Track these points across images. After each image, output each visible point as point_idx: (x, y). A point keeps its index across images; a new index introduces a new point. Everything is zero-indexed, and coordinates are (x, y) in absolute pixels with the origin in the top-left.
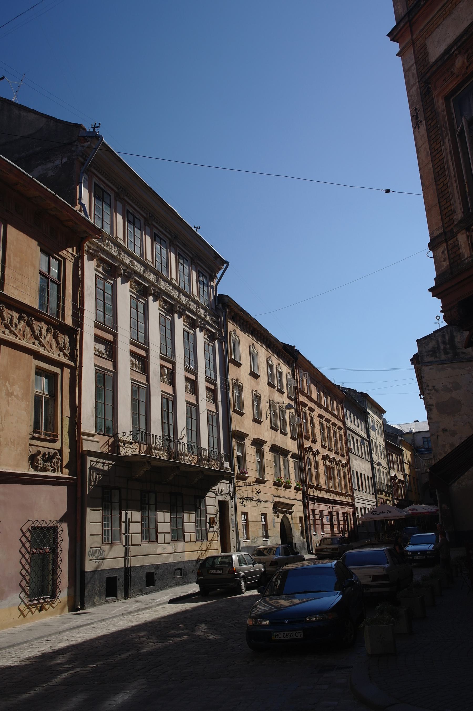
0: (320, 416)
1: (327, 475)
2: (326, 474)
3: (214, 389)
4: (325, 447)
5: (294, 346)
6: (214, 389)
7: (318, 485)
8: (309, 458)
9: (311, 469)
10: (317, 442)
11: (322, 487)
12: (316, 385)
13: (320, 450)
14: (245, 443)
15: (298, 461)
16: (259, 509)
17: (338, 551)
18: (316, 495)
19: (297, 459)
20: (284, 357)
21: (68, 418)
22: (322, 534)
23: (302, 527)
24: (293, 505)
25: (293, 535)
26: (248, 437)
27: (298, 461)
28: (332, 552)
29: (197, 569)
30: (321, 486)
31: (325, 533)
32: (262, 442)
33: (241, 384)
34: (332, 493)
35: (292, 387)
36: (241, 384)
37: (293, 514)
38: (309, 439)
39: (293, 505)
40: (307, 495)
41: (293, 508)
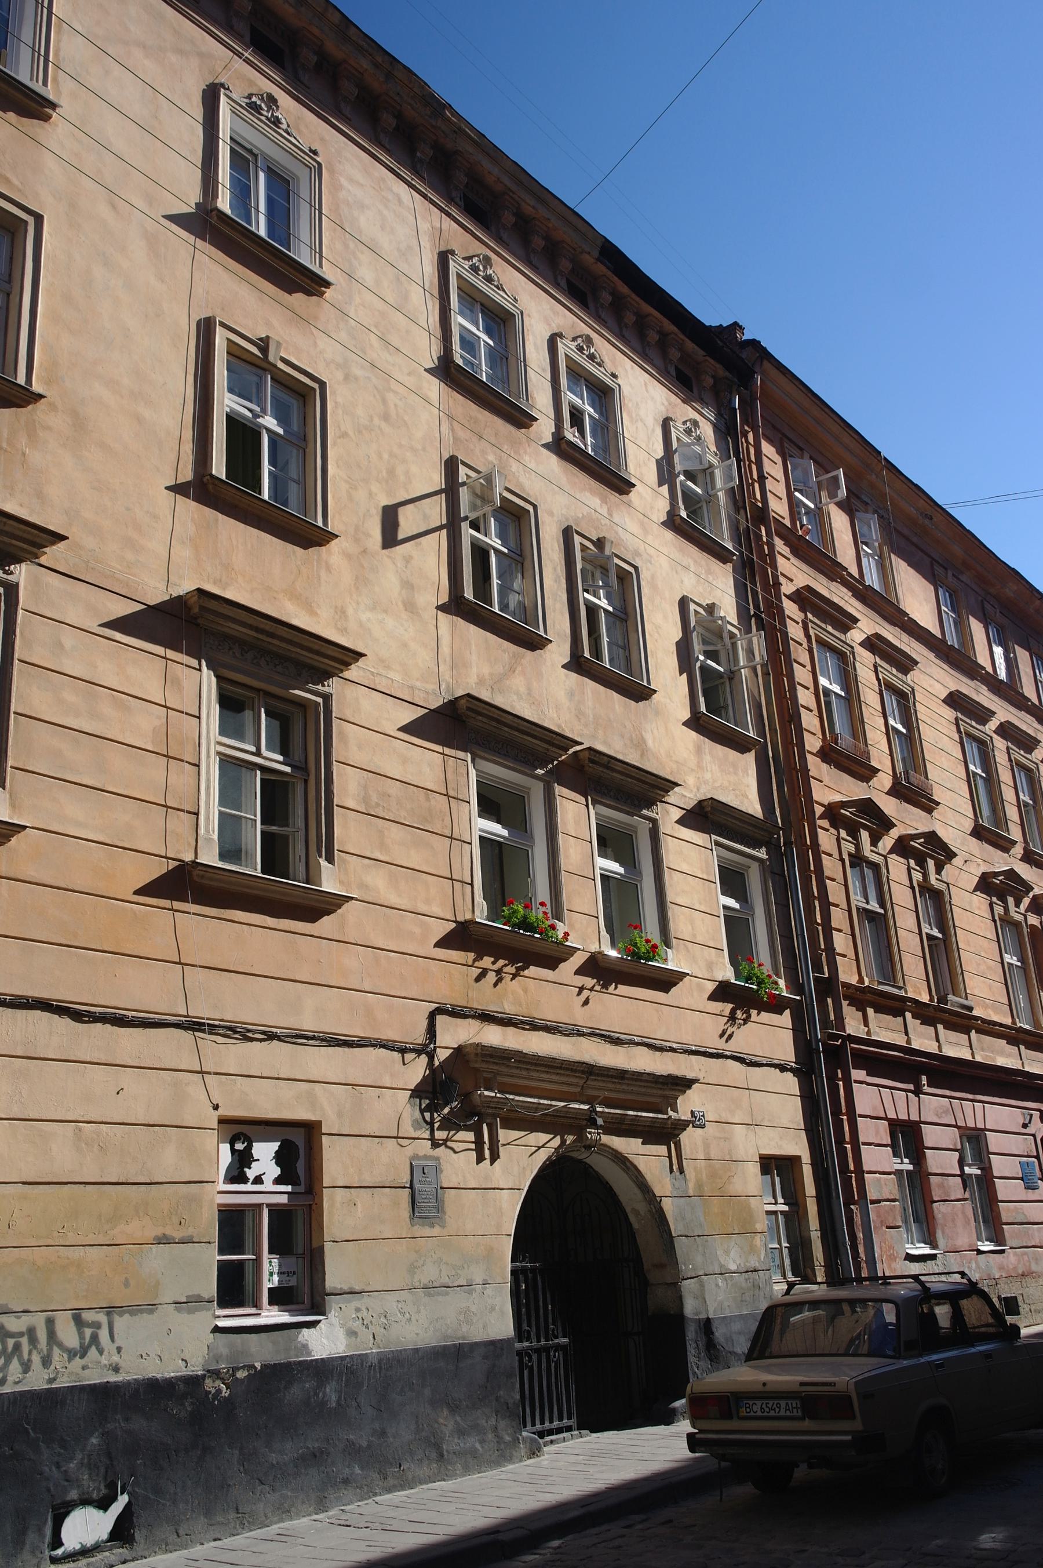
0: (1006, 730)
1: (1024, 968)
2: (1011, 959)
3: (685, 674)
4: (1008, 845)
5: (736, 326)
6: (685, 674)
7: (943, 999)
8: (875, 867)
9: (885, 916)
10: (938, 804)
11: (975, 1013)
12: (934, 575)
13: (889, 806)
14: (327, 698)
15: (765, 857)
16: (762, 1120)
17: (857, 1425)
18: (950, 1052)
19: (755, 844)
20: (642, 336)
21: (838, 950)
22: (980, 1252)
23: (795, 1218)
24: (684, 1084)
25: (686, 1268)
26: (673, 797)
27: (762, 854)
28: (807, 1424)
29: (88, 1493)
30: (971, 1009)
31: (1011, 1242)
32: (318, 653)
33: (631, 570)
34: (979, 1031)
35: (721, 495)
36: (631, 570)
37: (689, 1138)
38: (1008, 845)
39: (684, 1084)
40: (836, 1037)
41: (687, 1104)
